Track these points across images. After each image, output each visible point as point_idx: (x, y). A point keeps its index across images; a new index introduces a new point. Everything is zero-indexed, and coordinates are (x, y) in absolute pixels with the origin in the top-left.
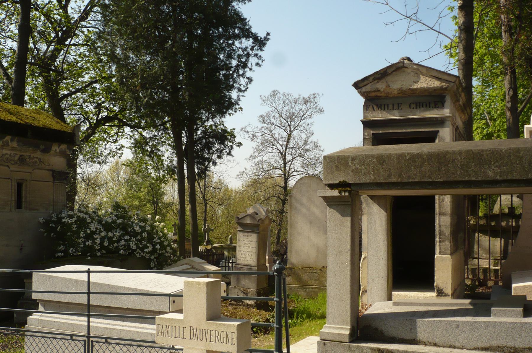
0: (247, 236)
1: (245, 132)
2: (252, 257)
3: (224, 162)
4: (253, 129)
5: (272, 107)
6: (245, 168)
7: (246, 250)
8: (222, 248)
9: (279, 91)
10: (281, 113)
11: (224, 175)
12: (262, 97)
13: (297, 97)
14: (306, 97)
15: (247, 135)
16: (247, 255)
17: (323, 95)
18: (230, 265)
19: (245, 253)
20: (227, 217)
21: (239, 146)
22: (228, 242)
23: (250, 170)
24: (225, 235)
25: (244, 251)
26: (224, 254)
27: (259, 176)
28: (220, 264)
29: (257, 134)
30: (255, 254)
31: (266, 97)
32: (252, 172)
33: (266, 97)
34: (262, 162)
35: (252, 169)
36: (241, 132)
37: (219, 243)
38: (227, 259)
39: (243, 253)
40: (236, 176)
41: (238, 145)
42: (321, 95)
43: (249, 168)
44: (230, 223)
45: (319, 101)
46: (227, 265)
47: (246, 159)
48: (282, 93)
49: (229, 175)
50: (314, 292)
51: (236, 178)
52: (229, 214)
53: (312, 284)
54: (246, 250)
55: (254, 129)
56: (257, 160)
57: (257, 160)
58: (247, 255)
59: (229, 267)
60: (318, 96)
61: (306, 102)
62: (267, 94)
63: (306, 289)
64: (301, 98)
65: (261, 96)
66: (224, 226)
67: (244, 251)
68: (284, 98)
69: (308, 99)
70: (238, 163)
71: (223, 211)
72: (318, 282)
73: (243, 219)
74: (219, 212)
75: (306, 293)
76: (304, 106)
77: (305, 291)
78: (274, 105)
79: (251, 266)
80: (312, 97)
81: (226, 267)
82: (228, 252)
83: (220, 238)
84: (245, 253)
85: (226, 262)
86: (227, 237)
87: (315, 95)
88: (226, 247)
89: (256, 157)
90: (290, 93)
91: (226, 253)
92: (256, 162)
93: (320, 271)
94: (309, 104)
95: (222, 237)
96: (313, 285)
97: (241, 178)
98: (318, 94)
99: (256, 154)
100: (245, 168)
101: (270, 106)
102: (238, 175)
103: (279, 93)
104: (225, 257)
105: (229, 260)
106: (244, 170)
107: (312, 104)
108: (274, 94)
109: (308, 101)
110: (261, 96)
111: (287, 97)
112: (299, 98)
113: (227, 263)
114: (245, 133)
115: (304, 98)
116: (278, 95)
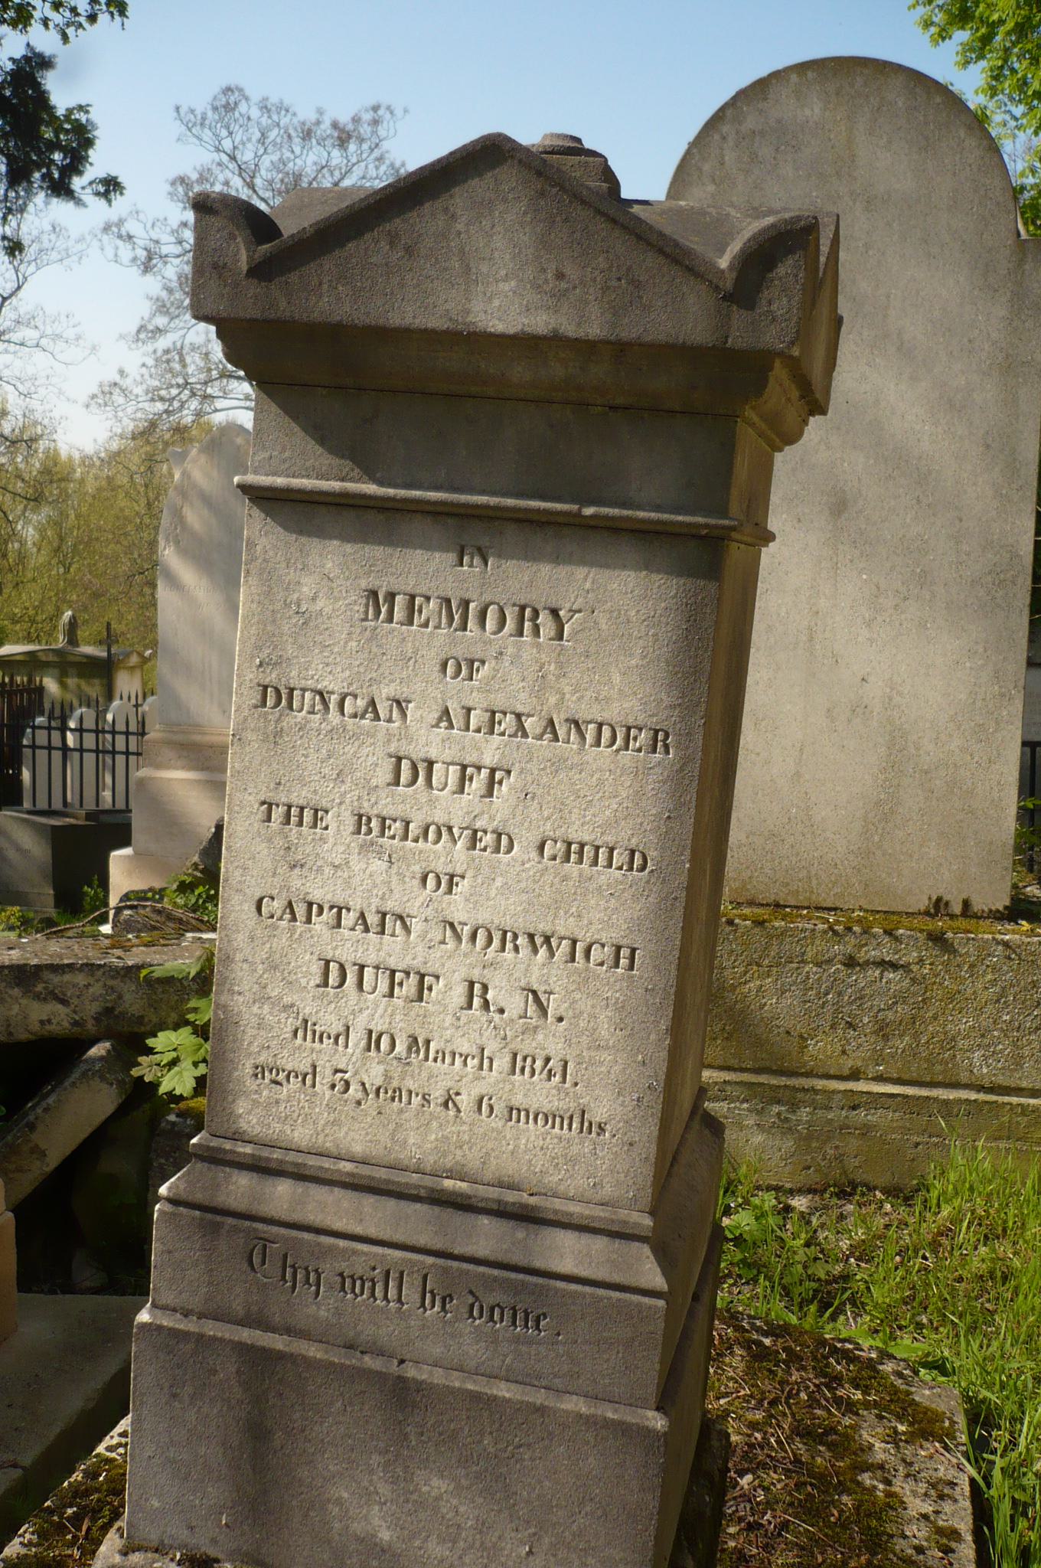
0: (456, 612)
1: (120, 237)
2: (551, 1042)
3: (44, 342)
4: (149, 225)
5: (218, 150)
6: (121, 372)
7: (416, 901)
8: (32, 662)
9: (247, 92)
10: (252, 177)
11: (42, 391)
12: (182, 111)
13: (312, 117)
14: (344, 119)
15: (126, 252)
16: (448, 993)
17: (406, 111)
18: (71, 739)
19: (392, 949)
20: (58, 549)
21: (106, 195)
22: (61, 641)
23: (139, 378)
24: (50, 608)
25: (384, 922)
26: (41, 690)
27: (171, 400)
28: (23, 734)
29: (165, 250)
30: (612, 983)
31: (198, 112)
32: (144, 387)
33: (198, 112)
34: (181, 354)
35: (147, 377)
36: (105, 237)
37: (29, 639)
38: (57, 712)
39: (350, 946)
40: (84, 398)
41: (102, 189)
42: (399, 112)
43: (134, 370)
44: (67, 570)
45: (392, 132)
46: (56, 740)
47: (122, 337)
48: (255, 96)
49: (61, 392)
50: (866, 1130)
51: (87, 406)
52: (61, 539)
53: (848, 1064)
54: (416, 901)
55: (153, 225)
56: (163, 343)
57: (163, 343)
58: (448, 993)
59: (65, 749)
60: (388, 116)
61: (343, 137)
62: (201, 100)
63: (794, 1107)
64: (326, 125)
65: (177, 109)
66: (45, 581)
67: (384, 922)
68: (264, 121)
69: (350, 127)
70: (94, 348)
71: (41, 530)
72: (902, 1043)
73: (373, 248)
74: (30, 533)
75: (789, 1144)
76: (336, 153)
77: (784, 1126)
78: (227, 144)
79: (527, 1217)
80: (367, 117)
81: (50, 748)
82: (63, 685)
83: (33, 621)
84: (392, 949)
85: (49, 728)
86: (59, 613)
87: (381, 112)
88: (51, 658)
89: (159, 331)
90: (286, 102)
91: (51, 685)
92: (159, 353)
93: (930, 952)
94: (352, 147)
95: (39, 618)
96: (855, 1075)
97: (106, 405)
98: (388, 108)
99: (161, 321)
100: (121, 372)
101: (213, 149)
102: (94, 397)
103: (247, 99)
104: (47, 706)
105: (64, 719)
106: (117, 378)
107: (365, 146)
108: (228, 102)
109: (349, 137)
110: (177, 109)
111: (275, 117)
112: (318, 123)
113: (56, 736)
114: (120, 243)
115: (335, 125)
116: (243, 107)
